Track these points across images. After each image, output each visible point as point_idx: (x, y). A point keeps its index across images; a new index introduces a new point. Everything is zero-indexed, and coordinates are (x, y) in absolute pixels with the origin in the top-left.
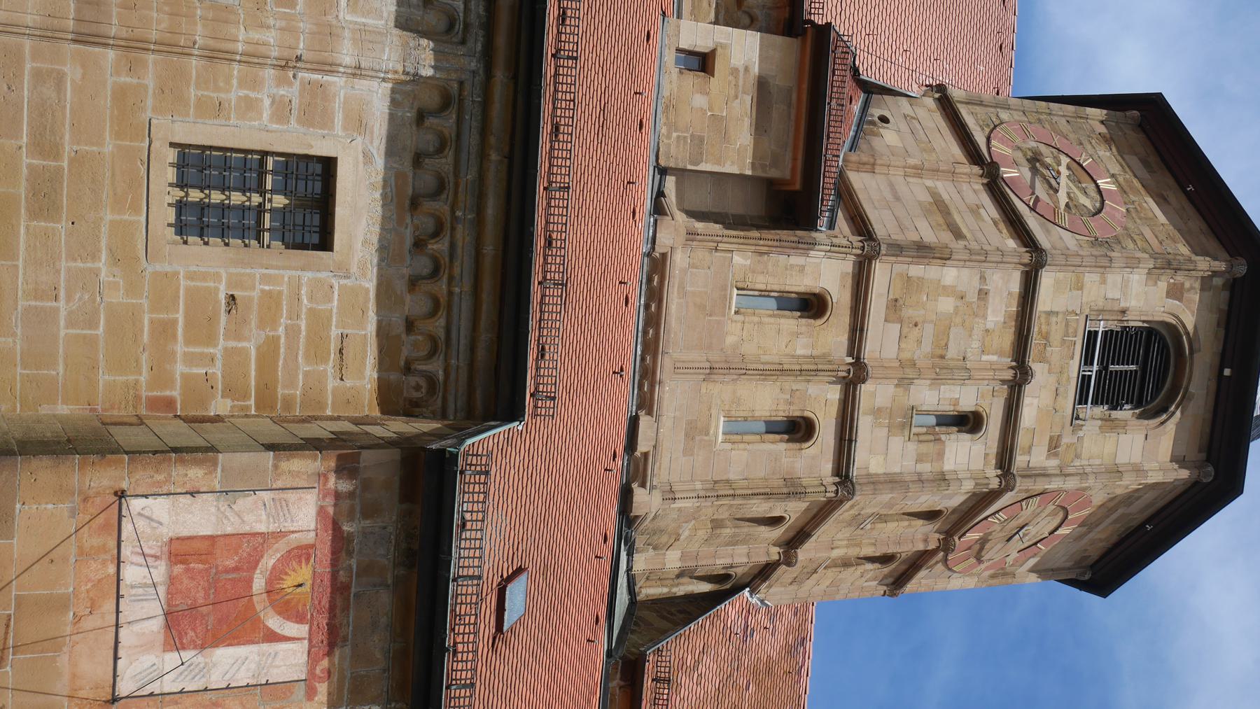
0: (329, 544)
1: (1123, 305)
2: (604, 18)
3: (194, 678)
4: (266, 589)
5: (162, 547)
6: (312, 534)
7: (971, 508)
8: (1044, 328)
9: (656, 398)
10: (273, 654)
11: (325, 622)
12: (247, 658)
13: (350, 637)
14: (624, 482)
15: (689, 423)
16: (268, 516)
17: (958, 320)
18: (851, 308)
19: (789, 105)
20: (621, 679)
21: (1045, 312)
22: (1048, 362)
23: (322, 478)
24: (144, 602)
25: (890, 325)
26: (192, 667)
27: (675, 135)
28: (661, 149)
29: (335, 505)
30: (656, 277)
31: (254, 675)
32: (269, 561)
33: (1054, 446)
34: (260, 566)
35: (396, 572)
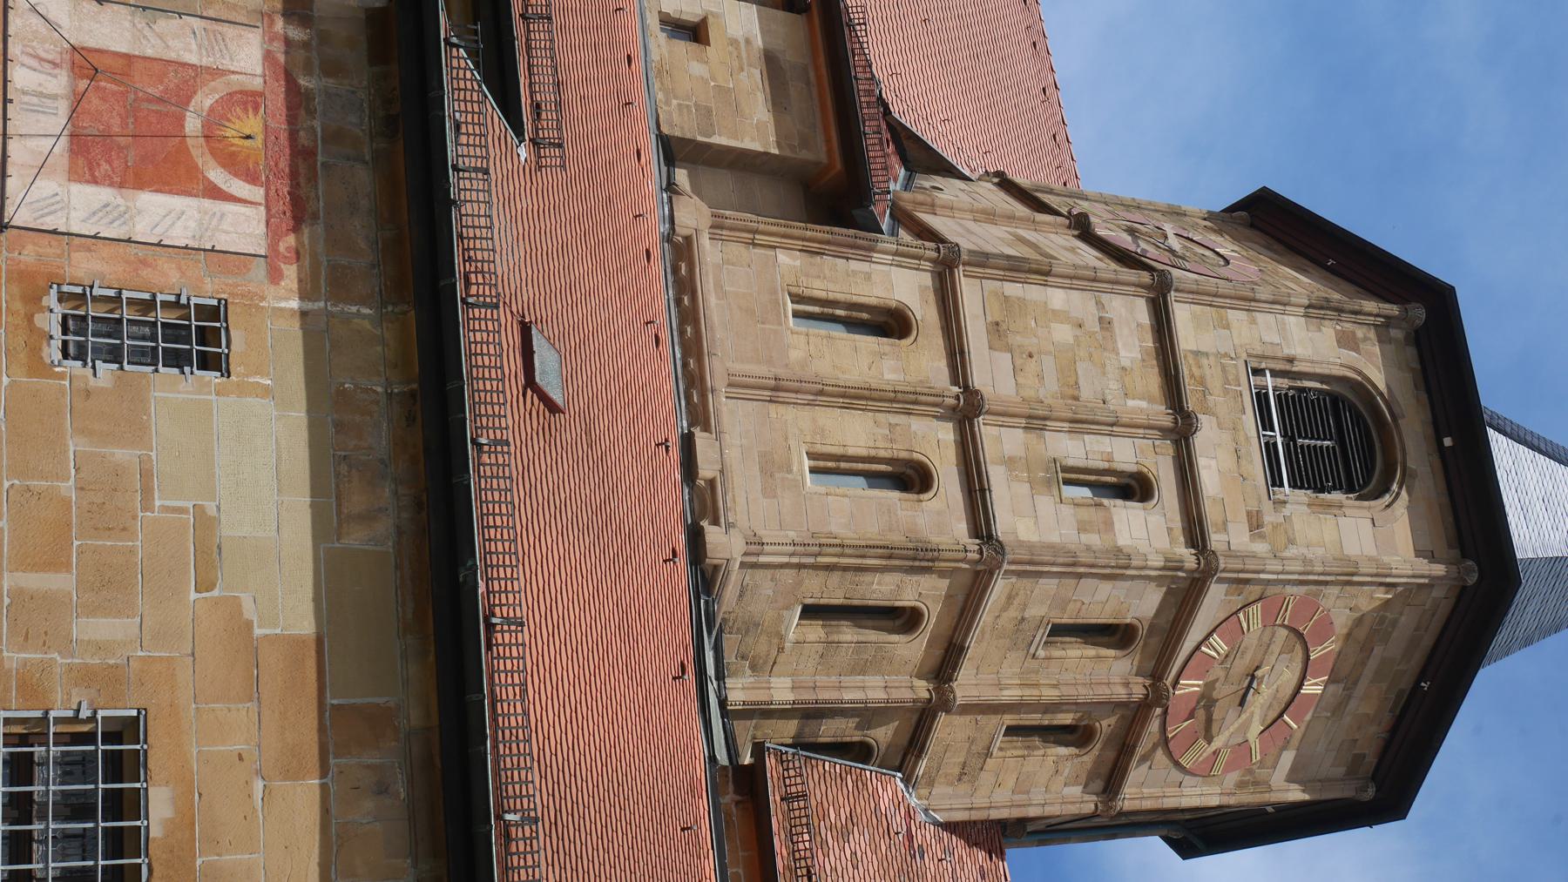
0: (282, 96)
1: (1287, 351)
2: (613, 750)
3: (111, 223)
4: (203, 132)
5: (61, 53)
6: (260, 81)
7: (1174, 620)
8: (1196, 372)
9: (712, 410)
10: (218, 215)
11: (286, 190)
12: (183, 213)
13: (321, 214)
14: (689, 522)
15: (763, 455)
16: (200, 47)
17: (1082, 353)
18: (942, 328)
19: (808, 83)
20: (736, 792)
21: (1191, 352)
22: (1213, 414)
23: (266, 19)
24: (40, 114)
25: (997, 354)
26: (108, 209)
27: (675, 102)
28: (661, 116)
29: (286, 53)
30: (683, 265)
31: (194, 237)
32: (205, 100)
33: (1255, 523)
34: (193, 103)
35: (374, 145)
